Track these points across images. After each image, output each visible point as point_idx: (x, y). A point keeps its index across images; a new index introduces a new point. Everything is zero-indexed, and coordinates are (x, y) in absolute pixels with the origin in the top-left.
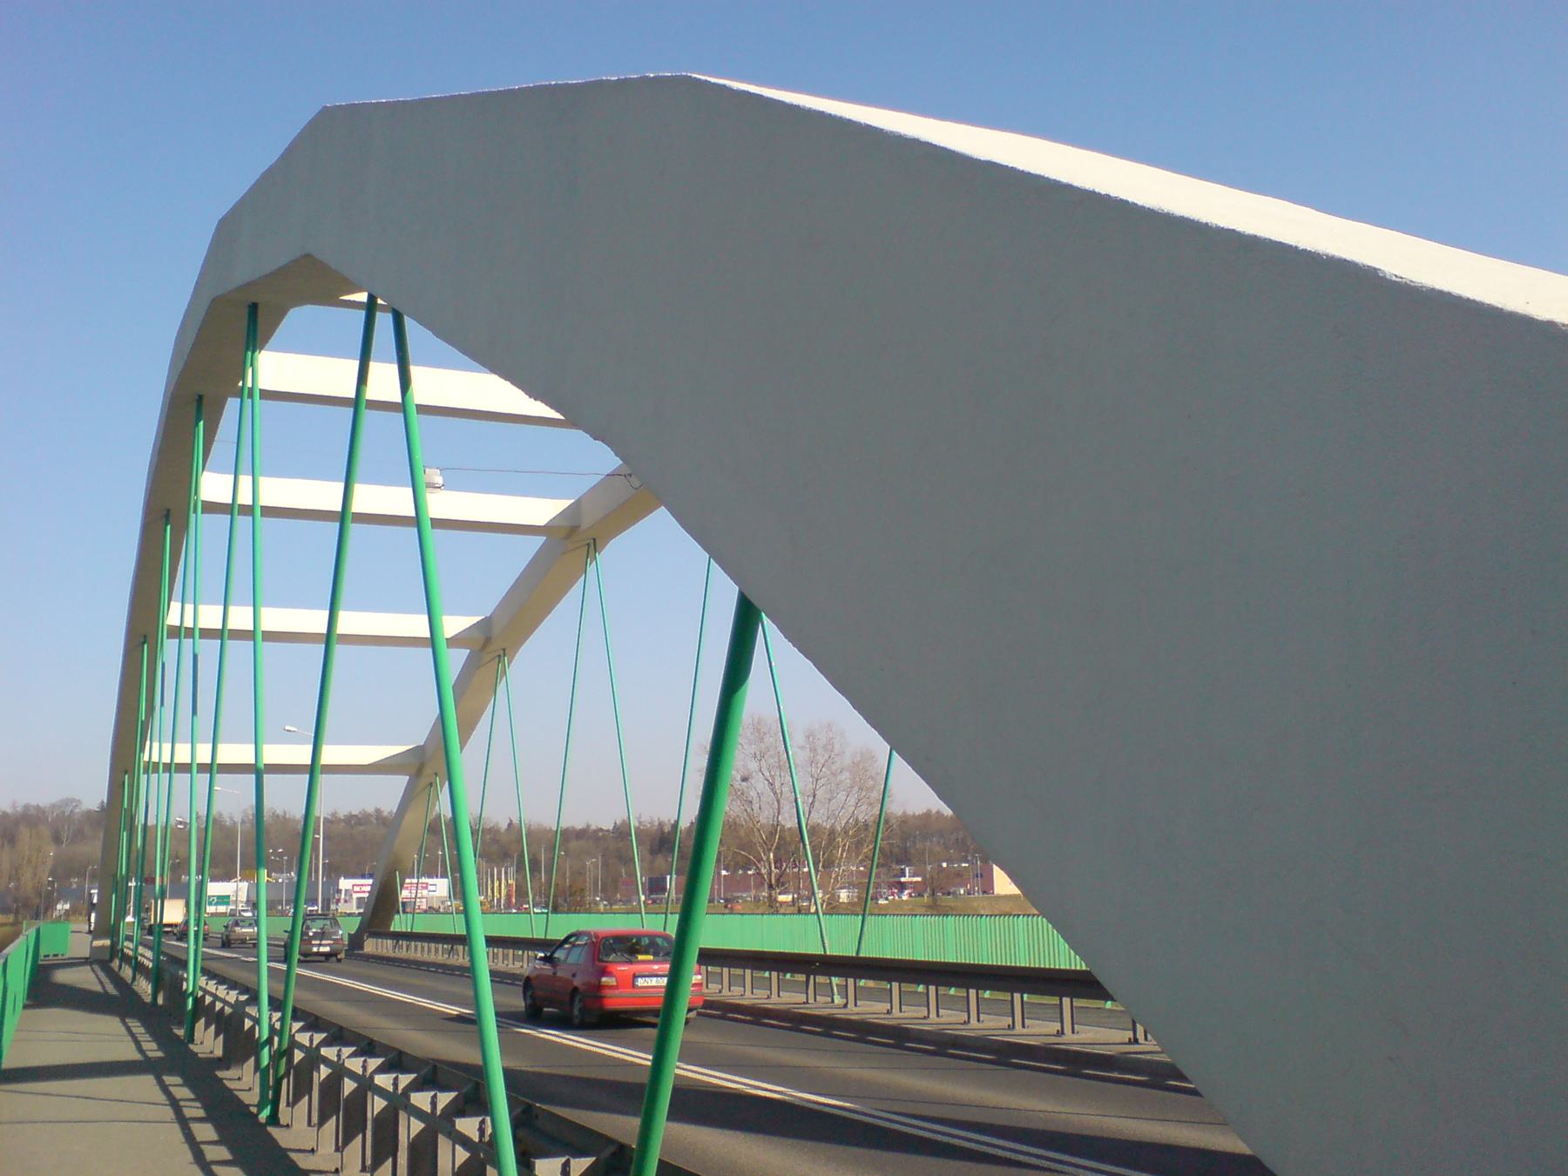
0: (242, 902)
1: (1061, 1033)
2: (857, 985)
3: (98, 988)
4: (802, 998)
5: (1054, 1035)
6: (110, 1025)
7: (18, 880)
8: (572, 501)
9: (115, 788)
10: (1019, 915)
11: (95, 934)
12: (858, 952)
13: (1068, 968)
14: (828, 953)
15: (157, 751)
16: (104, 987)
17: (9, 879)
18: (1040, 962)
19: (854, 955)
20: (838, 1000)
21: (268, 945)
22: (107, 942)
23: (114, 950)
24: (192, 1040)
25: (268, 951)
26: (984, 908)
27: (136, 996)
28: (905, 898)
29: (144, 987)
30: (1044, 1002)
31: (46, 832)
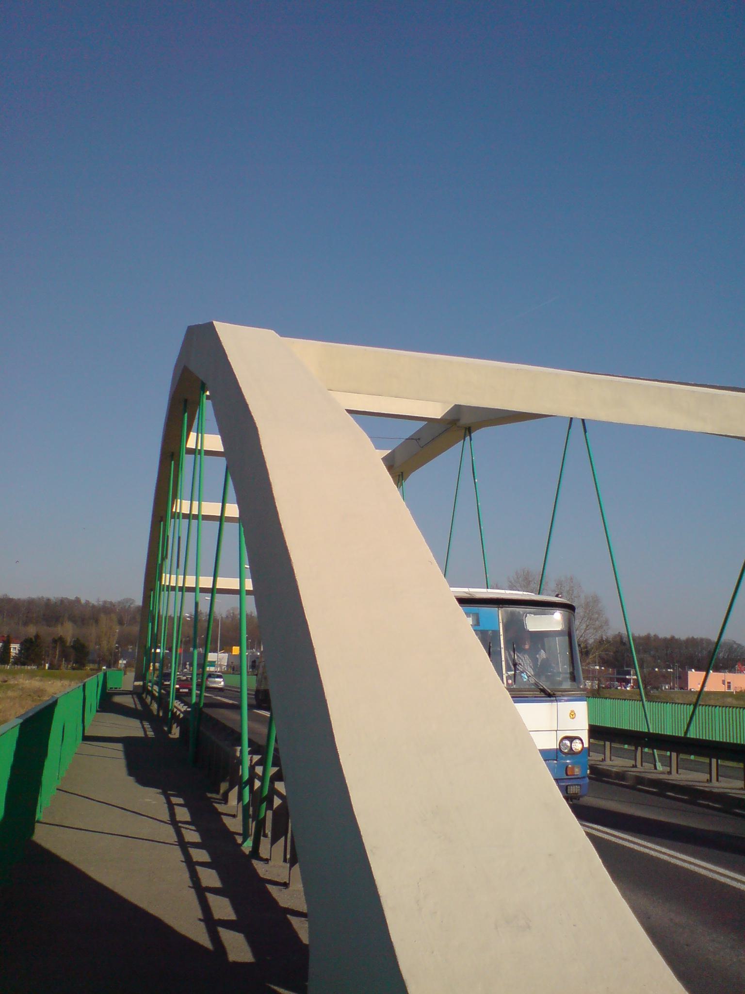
0: (224, 665)
1: (604, 760)
2: (643, 750)
3: (133, 706)
4: (601, 757)
5: (631, 767)
6: (136, 723)
7: (100, 645)
8: (390, 451)
9: (146, 598)
10: (716, 706)
11: (136, 680)
12: (686, 733)
13: (671, 734)
14: (651, 731)
15: (169, 579)
16: (136, 706)
17: (96, 644)
18: (730, 738)
19: (683, 735)
20: (659, 765)
21: (248, 694)
22: (141, 683)
23: (144, 687)
24: (170, 733)
25: (248, 698)
26: (678, 699)
27: (151, 711)
28: (628, 689)
29: (154, 707)
30: (701, 760)
31: (114, 617)
